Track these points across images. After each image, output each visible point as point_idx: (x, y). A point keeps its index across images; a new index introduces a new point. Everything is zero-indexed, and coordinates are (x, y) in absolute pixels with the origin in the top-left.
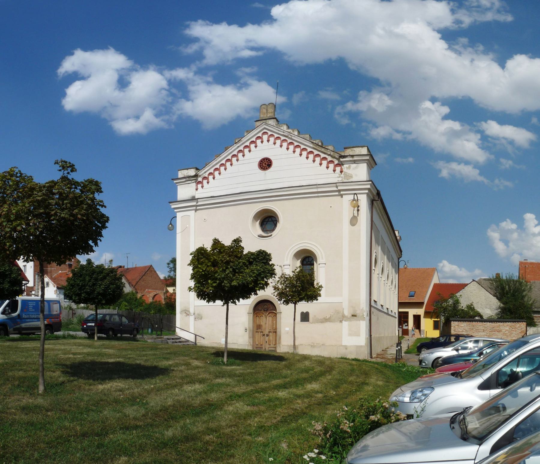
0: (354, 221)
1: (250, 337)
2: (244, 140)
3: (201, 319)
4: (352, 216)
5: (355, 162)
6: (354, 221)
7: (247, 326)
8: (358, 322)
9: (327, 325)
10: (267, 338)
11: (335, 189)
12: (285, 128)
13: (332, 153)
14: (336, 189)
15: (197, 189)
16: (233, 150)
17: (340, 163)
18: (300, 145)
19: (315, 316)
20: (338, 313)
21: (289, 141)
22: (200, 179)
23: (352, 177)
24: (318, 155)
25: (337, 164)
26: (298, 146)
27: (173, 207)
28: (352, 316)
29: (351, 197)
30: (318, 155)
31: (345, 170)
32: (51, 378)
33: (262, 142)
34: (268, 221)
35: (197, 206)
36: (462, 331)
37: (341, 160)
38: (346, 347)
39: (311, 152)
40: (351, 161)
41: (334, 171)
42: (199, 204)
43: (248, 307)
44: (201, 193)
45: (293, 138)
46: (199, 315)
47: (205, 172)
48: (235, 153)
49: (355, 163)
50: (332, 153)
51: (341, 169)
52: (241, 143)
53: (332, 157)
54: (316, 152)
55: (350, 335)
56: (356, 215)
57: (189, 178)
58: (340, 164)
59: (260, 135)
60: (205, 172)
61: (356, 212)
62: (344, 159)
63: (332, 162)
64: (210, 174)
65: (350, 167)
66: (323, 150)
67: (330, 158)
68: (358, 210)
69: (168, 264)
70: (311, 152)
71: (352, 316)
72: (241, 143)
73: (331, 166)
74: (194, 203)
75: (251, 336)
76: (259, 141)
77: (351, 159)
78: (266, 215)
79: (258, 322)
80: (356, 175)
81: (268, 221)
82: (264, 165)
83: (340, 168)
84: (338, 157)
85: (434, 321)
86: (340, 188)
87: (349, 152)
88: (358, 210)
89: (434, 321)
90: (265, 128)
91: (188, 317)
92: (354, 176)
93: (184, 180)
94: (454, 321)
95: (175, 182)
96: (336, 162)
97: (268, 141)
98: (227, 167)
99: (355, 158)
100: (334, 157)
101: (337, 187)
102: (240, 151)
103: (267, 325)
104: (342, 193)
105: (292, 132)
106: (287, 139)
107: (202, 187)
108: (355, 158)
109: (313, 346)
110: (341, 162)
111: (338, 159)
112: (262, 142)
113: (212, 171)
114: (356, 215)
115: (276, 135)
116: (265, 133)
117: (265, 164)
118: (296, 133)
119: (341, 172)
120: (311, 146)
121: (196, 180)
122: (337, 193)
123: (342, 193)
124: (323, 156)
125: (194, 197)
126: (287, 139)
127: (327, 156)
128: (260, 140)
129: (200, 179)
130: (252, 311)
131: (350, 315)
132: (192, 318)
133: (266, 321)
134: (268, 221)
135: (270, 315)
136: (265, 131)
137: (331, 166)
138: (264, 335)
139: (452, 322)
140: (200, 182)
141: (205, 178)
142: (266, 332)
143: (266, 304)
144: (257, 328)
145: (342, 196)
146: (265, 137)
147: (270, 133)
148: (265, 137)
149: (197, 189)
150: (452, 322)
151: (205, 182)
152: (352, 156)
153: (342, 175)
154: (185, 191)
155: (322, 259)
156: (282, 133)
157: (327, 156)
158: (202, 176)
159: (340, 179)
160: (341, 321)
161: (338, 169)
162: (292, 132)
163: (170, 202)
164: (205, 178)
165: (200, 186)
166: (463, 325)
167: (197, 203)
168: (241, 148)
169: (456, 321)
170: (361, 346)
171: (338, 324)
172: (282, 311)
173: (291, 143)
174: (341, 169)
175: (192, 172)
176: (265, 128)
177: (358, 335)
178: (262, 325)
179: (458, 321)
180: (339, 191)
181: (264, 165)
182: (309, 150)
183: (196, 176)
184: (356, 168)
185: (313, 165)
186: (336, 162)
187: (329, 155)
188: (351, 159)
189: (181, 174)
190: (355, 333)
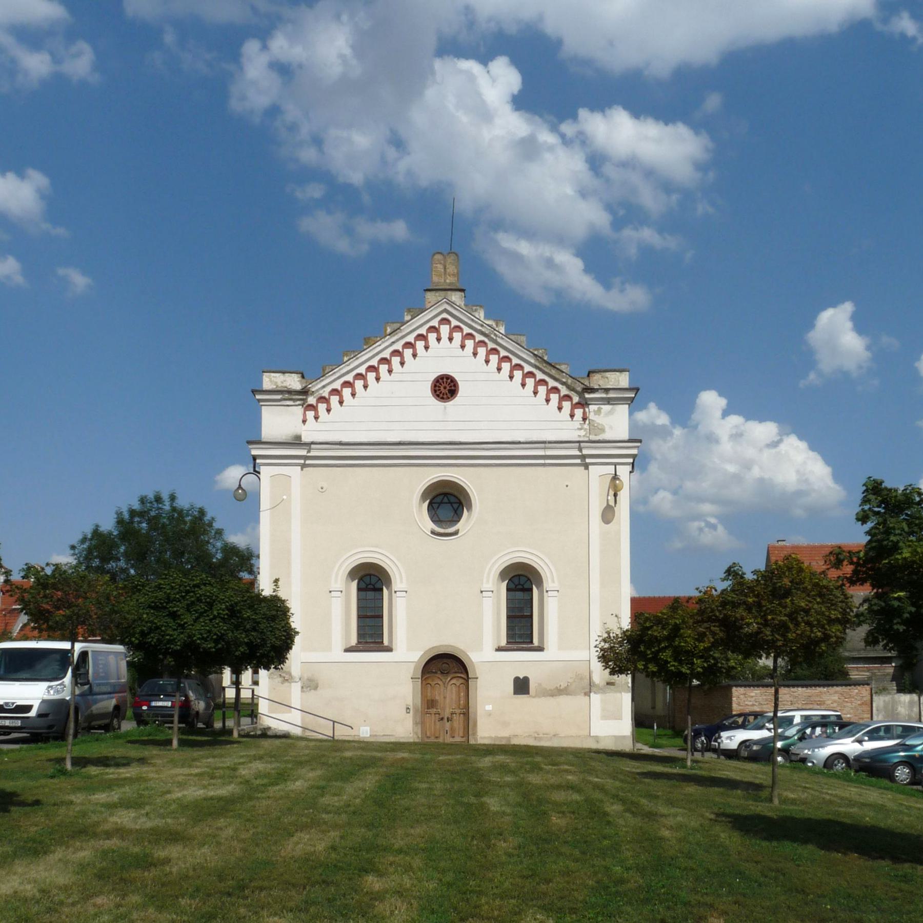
0: (608, 514)
1: (415, 723)
2: (406, 329)
3: (316, 688)
4: (605, 505)
5: (608, 401)
6: (608, 514)
7: (410, 701)
8: (618, 695)
9: (563, 700)
10: (448, 725)
12: (481, 314)
13: (570, 381)
14: (578, 453)
15: (304, 421)
16: (384, 348)
17: (583, 402)
18: (511, 356)
19: (540, 685)
20: (582, 679)
21: (491, 345)
22: (312, 400)
23: (603, 430)
24: (543, 382)
25: (577, 404)
26: (507, 359)
27: (254, 452)
28: (608, 684)
29: (611, 469)
30: (543, 382)
31: (592, 416)
33: (439, 340)
34: (447, 503)
35: (306, 458)
36: (753, 705)
37: (587, 396)
38: (597, 739)
39: (531, 374)
40: (602, 399)
41: (572, 416)
42: (312, 454)
43: (412, 666)
44: (311, 432)
45: (499, 340)
46: (310, 680)
47: (324, 387)
48: (386, 354)
49: (609, 404)
50: (570, 381)
51: (584, 413)
52: (400, 335)
53: (569, 387)
54: (540, 376)
55: (605, 717)
56: (612, 503)
57: (288, 394)
58: (583, 404)
59: (435, 323)
60: (324, 387)
61: (611, 498)
62: (592, 396)
63: (567, 397)
64: (335, 392)
65: (599, 410)
66: (553, 372)
67: (564, 391)
68: (615, 495)
69: (48, 564)
70: (531, 374)
71: (608, 684)
72: (400, 335)
74: (303, 452)
75: (418, 720)
76: (432, 337)
77: (604, 395)
78: (447, 490)
79: (429, 694)
80: (611, 428)
81: (451, 503)
82: (442, 388)
83: (582, 410)
86: (585, 452)
87: (597, 381)
88: (615, 495)
90: (445, 311)
91: (286, 684)
92: (607, 429)
93: (279, 397)
94: (737, 686)
95: (258, 397)
96: (576, 399)
98: (332, 406)
99: (612, 395)
100: (573, 390)
101: (580, 449)
102: (396, 353)
103: (448, 700)
104: (588, 461)
105: (494, 326)
106: (486, 340)
107: (316, 418)
108: (612, 395)
110: (586, 399)
111: (581, 394)
112: (439, 340)
113: (337, 385)
114: (612, 503)
115: (467, 330)
116: (445, 321)
117: (445, 388)
118: (502, 330)
119: (584, 419)
120: (533, 361)
121: (305, 400)
122: (578, 461)
123: (588, 461)
124: (552, 383)
125: (298, 437)
126: (486, 340)
127: (560, 386)
128: (398, 359)
129: (312, 400)
130: (419, 675)
131: (603, 683)
132: (296, 688)
133: (447, 692)
134: (447, 503)
135: (454, 681)
136: (445, 315)
137: (567, 405)
138: (442, 719)
139: (734, 689)
140: (324, 398)
141: (322, 399)
142: (447, 714)
143: (445, 660)
144: (429, 705)
145: (586, 466)
146: (445, 330)
147: (454, 323)
148: (445, 330)
149: (304, 421)
150: (734, 689)
151: (322, 407)
152: (607, 390)
153: (586, 426)
154: (278, 421)
155: (553, 581)
156: (479, 328)
157: (560, 386)
158: (317, 395)
159: (582, 433)
160: (587, 694)
161: (579, 412)
162: (494, 326)
163: (249, 443)
164: (322, 399)
165: (310, 414)
166: (753, 694)
167: (309, 452)
168: (398, 346)
169: (741, 686)
170: (624, 737)
171: (581, 700)
172: (478, 675)
173: (494, 351)
175: (294, 382)
176: (445, 311)
177: (619, 717)
178: (437, 701)
179: (745, 686)
180: (583, 457)
181: (442, 388)
182: (528, 368)
183: (305, 392)
184: (610, 413)
185: (533, 399)
186: (576, 399)
187: (563, 383)
188: (604, 395)
189: (270, 381)
190: (612, 715)
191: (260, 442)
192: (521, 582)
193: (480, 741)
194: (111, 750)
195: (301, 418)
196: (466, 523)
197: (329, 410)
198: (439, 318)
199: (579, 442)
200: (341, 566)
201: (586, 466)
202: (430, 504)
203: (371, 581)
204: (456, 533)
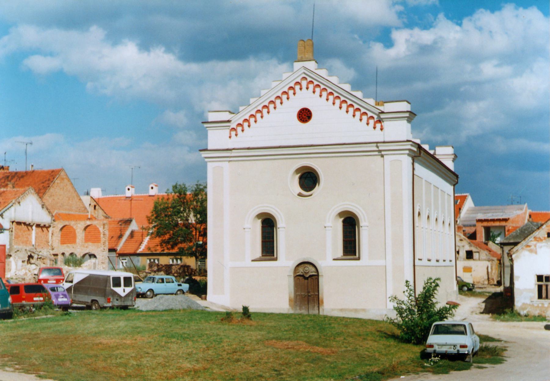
11: (376, 149)
15: (230, 137)
32: (199, 377)
33: (301, 89)
34: (309, 179)
51: (382, 126)
58: (380, 121)
73: (372, 122)
78: (309, 171)
84: (377, 113)
85: (4, 246)
86: (380, 148)
89: (4, 246)
90: (304, 73)
97: (307, 88)
98: (270, 110)
101: (377, 147)
109: (341, 310)
112: (301, 89)
122: (377, 153)
123: (383, 153)
134: (309, 179)
140: (234, 128)
145: (382, 156)
146: (304, 83)
148: (304, 83)
149: (230, 137)
155: (365, 221)
157: (367, 112)
161: (378, 126)
165: (233, 133)
172: (324, 275)
174: (382, 126)
180: (380, 151)
191: (206, 150)
192: (350, 223)
193: (325, 313)
194: (42, 141)
195: (229, 135)
196: (317, 190)
197: (256, 122)
198: (256, 110)
199: (377, 143)
200: (352, 205)
201: (382, 156)
202: (300, 178)
203: (268, 224)
204: (311, 195)
